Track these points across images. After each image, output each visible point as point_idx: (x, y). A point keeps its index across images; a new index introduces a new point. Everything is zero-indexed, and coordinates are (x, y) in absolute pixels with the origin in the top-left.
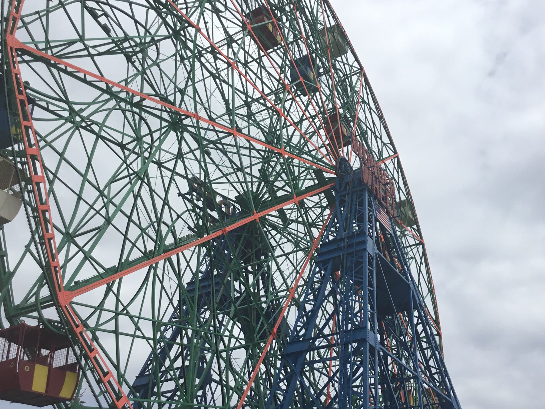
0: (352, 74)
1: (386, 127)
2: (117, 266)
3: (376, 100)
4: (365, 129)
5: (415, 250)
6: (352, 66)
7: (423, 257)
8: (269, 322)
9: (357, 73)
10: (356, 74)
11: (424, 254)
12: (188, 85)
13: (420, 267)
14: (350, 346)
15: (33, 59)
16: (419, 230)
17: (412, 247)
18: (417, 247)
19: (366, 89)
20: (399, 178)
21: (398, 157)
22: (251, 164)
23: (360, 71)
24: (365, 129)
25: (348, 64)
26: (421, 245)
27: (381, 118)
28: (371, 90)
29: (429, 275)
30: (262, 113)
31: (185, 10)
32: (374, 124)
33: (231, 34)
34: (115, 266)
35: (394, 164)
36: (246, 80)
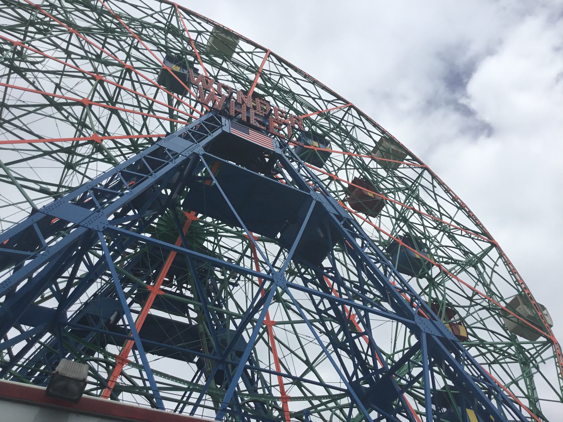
0: (169, 20)
6: (161, 11)
7: (361, 116)
11: (360, 113)
14: (71, 312)
15: (334, 316)
16: (414, 158)
19: (194, 21)
20: (363, 123)
21: (272, 53)
23: (173, 8)
25: (156, 12)
26: (352, 109)
27: (314, 82)
28: (198, 16)
29: (373, 123)
31: (85, 178)
32: (305, 90)
36: (22, 140)
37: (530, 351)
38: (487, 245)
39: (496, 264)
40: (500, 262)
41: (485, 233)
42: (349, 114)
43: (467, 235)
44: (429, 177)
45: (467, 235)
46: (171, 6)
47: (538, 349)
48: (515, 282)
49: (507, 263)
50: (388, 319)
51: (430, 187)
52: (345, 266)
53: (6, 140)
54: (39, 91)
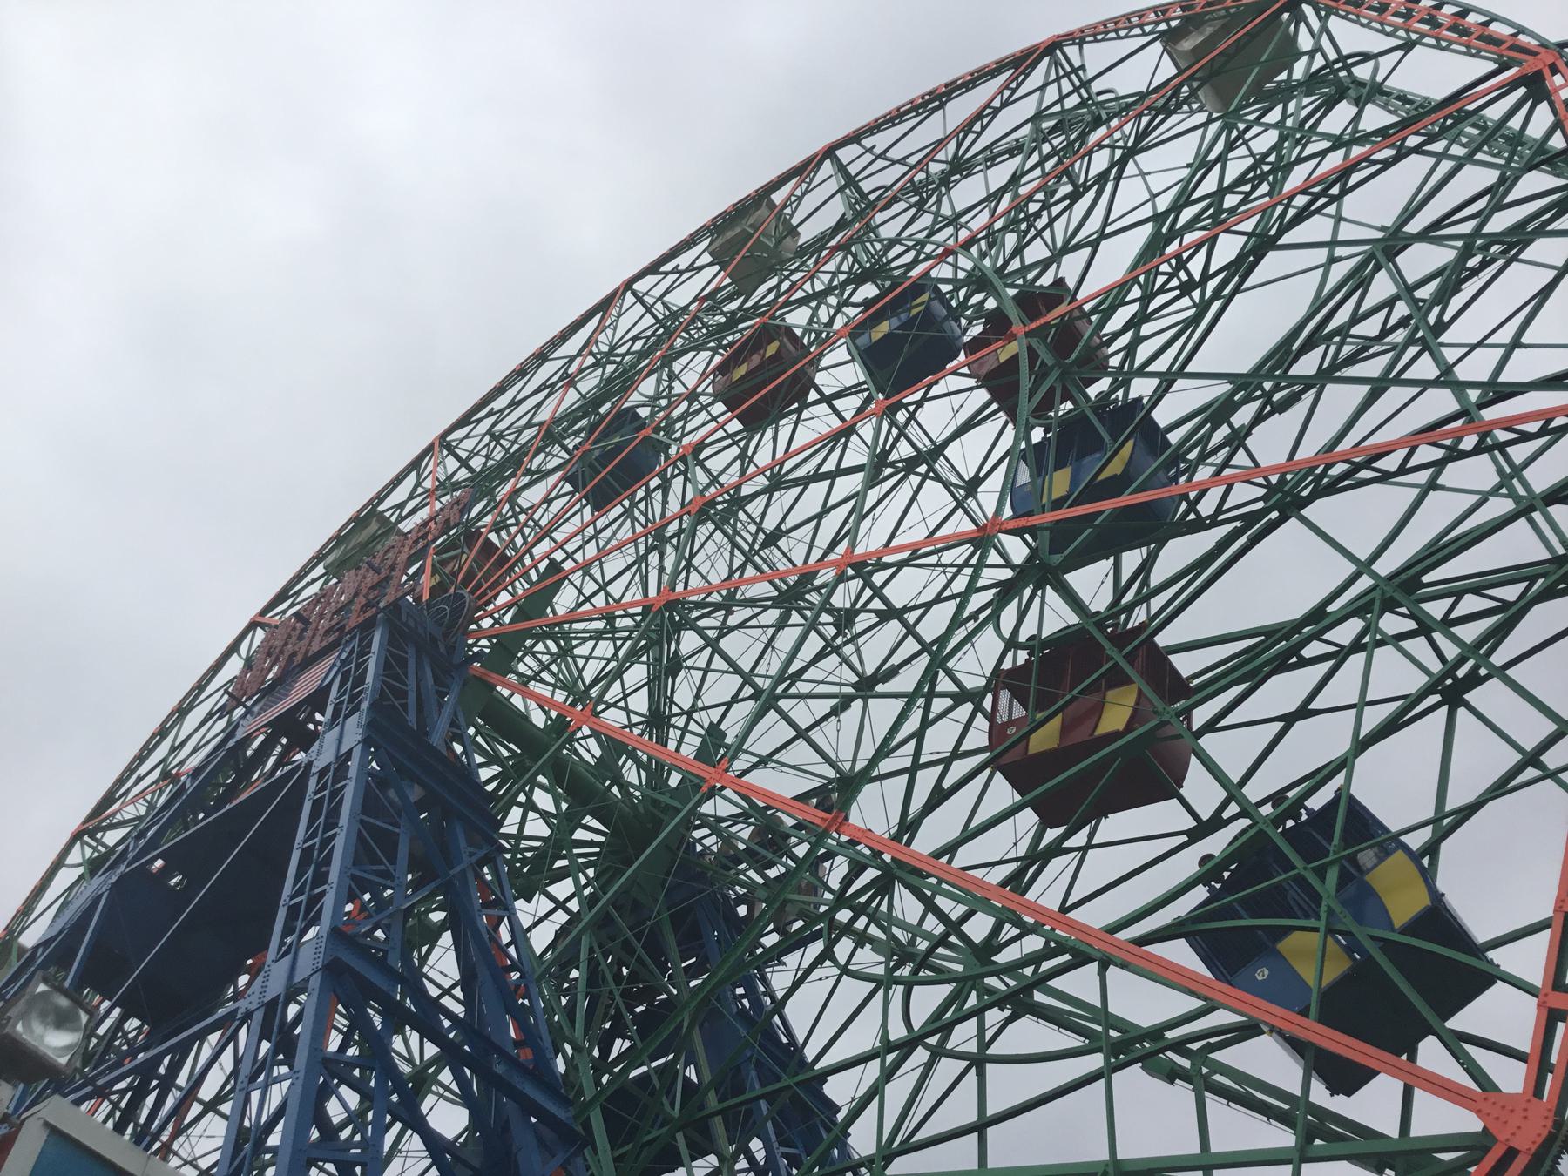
1: (200, 686)
2: (1140, 1064)
3: (142, 750)
4: (534, 430)
5: (468, 445)
8: (1048, 341)
9: (96, 840)
10: (99, 842)
12: (1325, 211)
13: (502, 411)
17: (464, 455)
18: (456, 447)
20: (314, 581)
21: (263, 613)
22: (1150, 192)
24: (534, 430)
27: (181, 711)
28: (121, 781)
30: (786, 551)
33: (946, 453)
34: (1142, 1067)
35: (461, 440)
37: (1064, 93)
38: (827, 167)
39: (870, 150)
40: (867, 142)
41: (604, 306)
42: (456, 447)
43: (794, 205)
44: (650, 280)
45: (794, 205)
46: (78, 844)
47: (1061, 73)
48: (918, 115)
49: (875, 128)
50: (861, 1093)
51: (672, 278)
52: (826, 510)
53: (950, 716)
54: (852, 532)
